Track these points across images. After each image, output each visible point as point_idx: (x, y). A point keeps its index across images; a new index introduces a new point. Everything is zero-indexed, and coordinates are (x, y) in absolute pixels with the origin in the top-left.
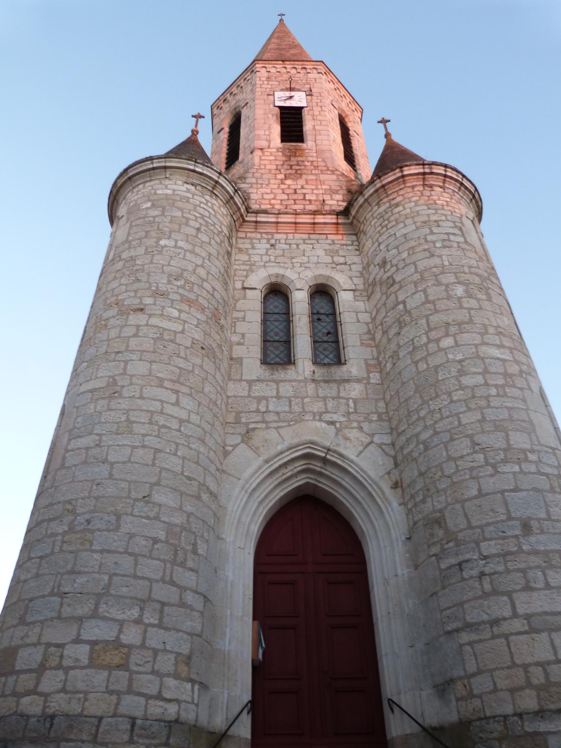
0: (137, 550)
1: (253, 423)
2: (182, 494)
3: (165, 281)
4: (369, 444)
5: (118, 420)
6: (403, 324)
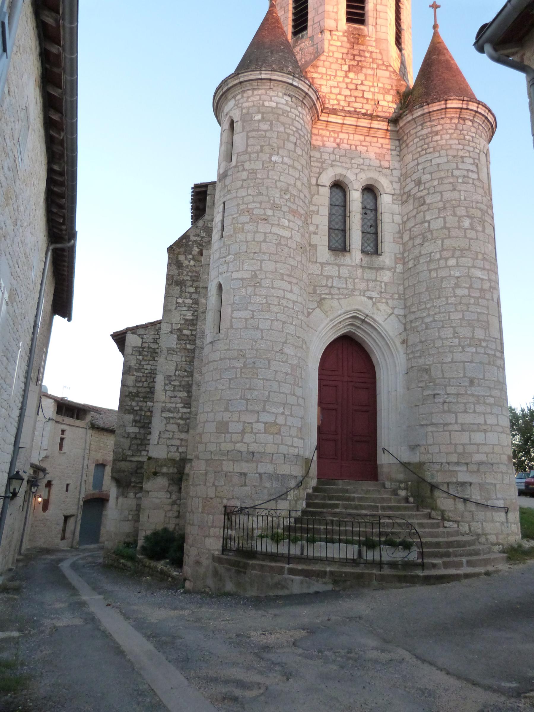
0: (279, 379)
1: (324, 294)
2: (296, 347)
3: (278, 195)
4: (391, 314)
5: (261, 302)
6: (426, 239)
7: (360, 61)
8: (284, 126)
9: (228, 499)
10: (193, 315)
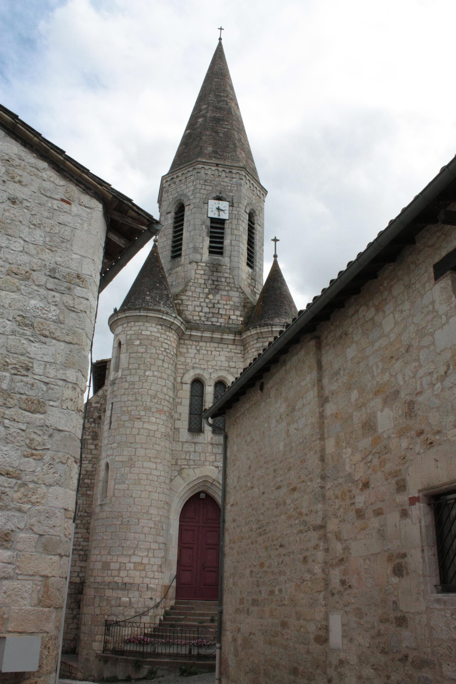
1: (183, 465)
2: (159, 508)
3: (149, 401)
7: (218, 285)
8: (156, 348)
9: (108, 616)
10: (92, 467)
